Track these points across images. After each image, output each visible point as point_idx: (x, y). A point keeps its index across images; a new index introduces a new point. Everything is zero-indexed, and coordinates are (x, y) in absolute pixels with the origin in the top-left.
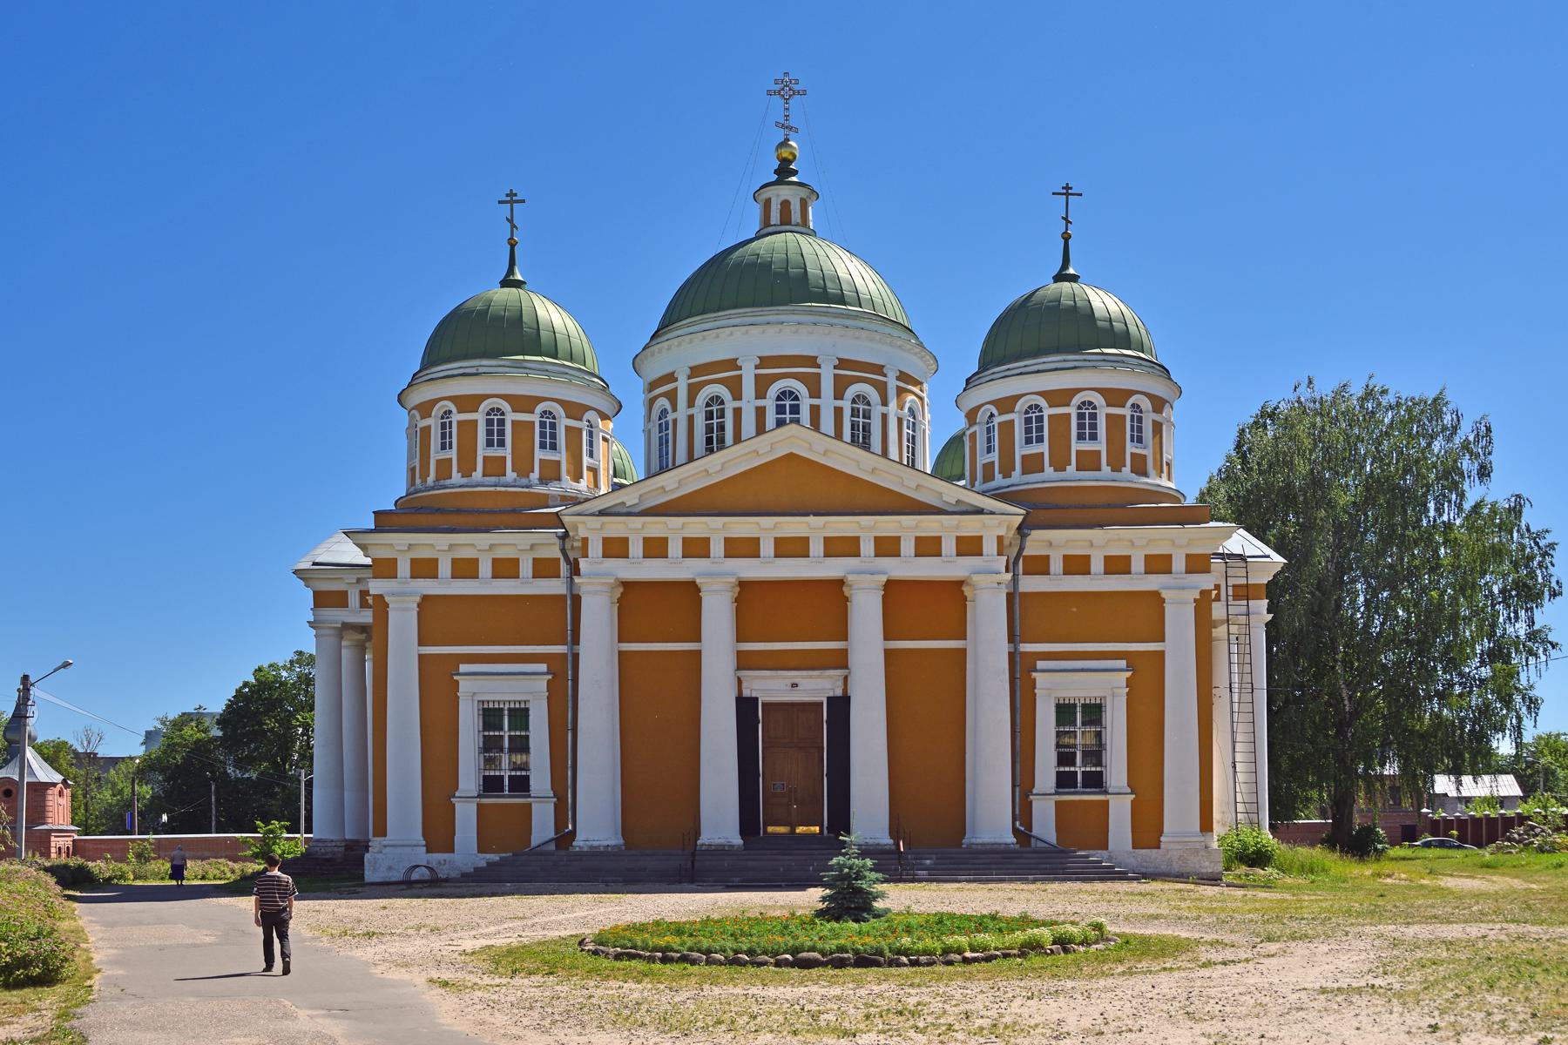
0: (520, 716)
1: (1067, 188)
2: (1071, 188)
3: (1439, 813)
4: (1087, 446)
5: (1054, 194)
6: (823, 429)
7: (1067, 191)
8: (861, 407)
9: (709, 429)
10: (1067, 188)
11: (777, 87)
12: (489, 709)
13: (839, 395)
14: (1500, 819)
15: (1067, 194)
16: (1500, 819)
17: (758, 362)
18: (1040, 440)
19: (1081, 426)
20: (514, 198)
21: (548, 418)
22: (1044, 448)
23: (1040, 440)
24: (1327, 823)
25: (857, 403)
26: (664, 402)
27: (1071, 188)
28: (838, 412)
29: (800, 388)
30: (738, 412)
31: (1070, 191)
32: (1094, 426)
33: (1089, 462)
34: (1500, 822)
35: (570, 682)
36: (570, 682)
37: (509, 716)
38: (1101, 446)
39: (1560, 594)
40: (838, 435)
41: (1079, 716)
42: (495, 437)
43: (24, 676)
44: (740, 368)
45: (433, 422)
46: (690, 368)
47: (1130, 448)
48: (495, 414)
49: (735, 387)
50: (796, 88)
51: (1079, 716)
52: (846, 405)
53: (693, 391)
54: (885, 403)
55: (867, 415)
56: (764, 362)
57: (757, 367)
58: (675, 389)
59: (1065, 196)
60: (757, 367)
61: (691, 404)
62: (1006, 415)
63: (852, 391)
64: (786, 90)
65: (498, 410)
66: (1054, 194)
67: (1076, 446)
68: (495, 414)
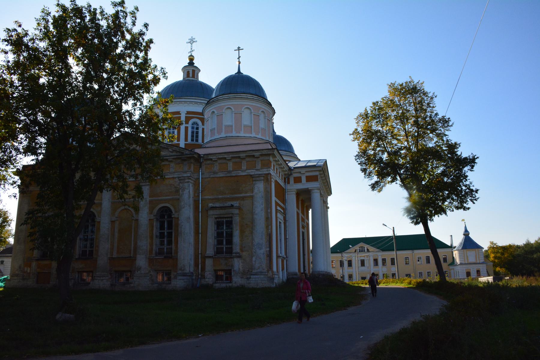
1: (239, 48)
2: (240, 48)
3: (112, 95)
5: (235, 50)
7: (239, 49)
8: (195, 126)
9: (193, 132)
10: (239, 48)
11: (189, 41)
13: (187, 122)
15: (239, 50)
17: (186, 112)
20: (240, 49)
24: (201, 212)
25: (194, 125)
27: (240, 48)
31: (240, 49)
37: (165, 228)
39: (409, 264)
41: (225, 235)
44: (180, 114)
46: (187, 111)
50: (194, 40)
51: (225, 235)
52: (190, 125)
53: (187, 120)
54: (203, 125)
55: (197, 128)
56: (188, 113)
59: (238, 51)
60: (186, 114)
64: (192, 41)
65: (196, 123)
66: (235, 50)
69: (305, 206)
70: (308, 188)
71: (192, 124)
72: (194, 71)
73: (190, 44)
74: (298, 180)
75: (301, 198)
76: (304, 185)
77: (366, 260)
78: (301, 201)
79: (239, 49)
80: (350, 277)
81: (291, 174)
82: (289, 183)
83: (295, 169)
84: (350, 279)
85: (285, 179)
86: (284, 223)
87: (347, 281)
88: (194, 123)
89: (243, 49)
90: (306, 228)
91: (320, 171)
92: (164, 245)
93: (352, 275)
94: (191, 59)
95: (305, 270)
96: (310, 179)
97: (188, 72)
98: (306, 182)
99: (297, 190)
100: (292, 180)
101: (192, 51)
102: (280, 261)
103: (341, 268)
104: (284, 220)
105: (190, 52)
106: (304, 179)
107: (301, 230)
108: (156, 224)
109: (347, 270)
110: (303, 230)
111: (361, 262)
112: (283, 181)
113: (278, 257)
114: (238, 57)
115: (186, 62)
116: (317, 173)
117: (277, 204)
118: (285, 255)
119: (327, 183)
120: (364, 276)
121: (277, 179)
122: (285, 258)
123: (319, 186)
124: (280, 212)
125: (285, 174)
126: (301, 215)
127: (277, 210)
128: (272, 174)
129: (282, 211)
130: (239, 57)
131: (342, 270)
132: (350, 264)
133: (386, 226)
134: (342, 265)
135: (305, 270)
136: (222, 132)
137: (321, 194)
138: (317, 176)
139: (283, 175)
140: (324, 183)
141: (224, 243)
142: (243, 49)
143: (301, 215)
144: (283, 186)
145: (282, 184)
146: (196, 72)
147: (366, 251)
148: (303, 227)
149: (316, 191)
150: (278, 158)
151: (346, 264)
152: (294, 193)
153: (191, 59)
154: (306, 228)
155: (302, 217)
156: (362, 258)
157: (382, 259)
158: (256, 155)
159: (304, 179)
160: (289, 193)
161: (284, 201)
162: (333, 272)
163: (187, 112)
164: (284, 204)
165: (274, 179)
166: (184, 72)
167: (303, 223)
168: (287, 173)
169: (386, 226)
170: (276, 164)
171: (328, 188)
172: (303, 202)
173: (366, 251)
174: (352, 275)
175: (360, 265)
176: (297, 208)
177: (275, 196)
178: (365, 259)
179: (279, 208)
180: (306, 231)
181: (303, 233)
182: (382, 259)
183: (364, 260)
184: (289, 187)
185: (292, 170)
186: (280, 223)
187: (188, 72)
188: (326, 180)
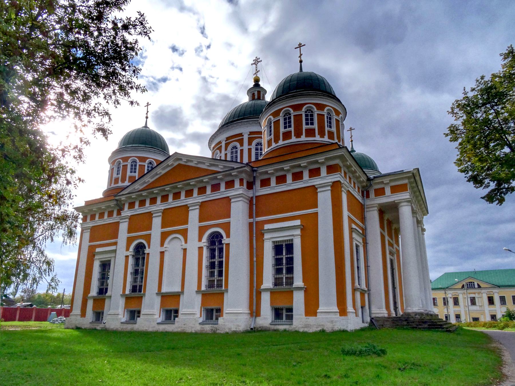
0: (290, 247)
1: (300, 44)
4: (310, 126)
6: (115, 249)
10: (300, 44)
11: (254, 62)
12: (277, 278)
14: (254, 217)
16: (254, 217)
17: (249, 133)
18: (135, 172)
19: (307, 120)
21: (309, 112)
22: (292, 129)
23: (135, 172)
26: (218, 151)
28: (250, 150)
29: (238, 144)
30: (242, 151)
32: (312, 120)
33: (310, 133)
34: (254, 215)
35: (254, 203)
36: (254, 203)
38: (316, 126)
40: (115, 244)
42: (134, 170)
43: (252, 188)
45: (129, 163)
47: (327, 129)
48: (309, 110)
49: (241, 142)
50: (259, 60)
53: (227, 145)
56: (251, 133)
57: (249, 135)
58: (221, 146)
61: (226, 149)
62: (278, 224)
63: (254, 143)
67: (305, 127)
68: (309, 110)
69: (393, 228)
70: (394, 201)
71: (256, 145)
72: (259, 92)
73: (254, 65)
74: (380, 192)
75: (386, 217)
76: (388, 198)
77: (478, 298)
78: (387, 220)
79: (300, 46)
80: (458, 317)
81: (371, 185)
82: (368, 196)
83: (376, 179)
84: (457, 319)
85: (363, 192)
86: (364, 246)
87: (453, 320)
88: (258, 144)
89: (305, 45)
90: (395, 255)
91: (409, 178)
92: (214, 276)
93: (459, 315)
94: (257, 81)
95: (397, 308)
96: (395, 189)
97: (254, 94)
98: (392, 193)
99: (379, 204)
100: (372, 194)
101: (258, 72)
102: (358, 295)
103: (445, 307)
104: (363, 242)
105: (255, 73)
106: (388, 190)
107: (388, 257)
108: (206, 253)
109: (452, 310)
110: (392, 257)
111: (471, 300)
112: (361, 194)
113: (354, 290)
114: (299, 55)
115: (252, 84)
116: (406, 181)
117: (351, 221)
118: (366, 287)
119: (415, 183)
120: (476, 317)
121: (349, 189)
122: (366, 291)
123: (408, 197)
124: (356, 231)
125: (363, 187)
126: (387, 238)
127: (351, 230)
128: (342, 182)
129: (361, 231)
130: (301, 55)
131: (446, 309)
132: (456, 302)
133: (511, 251)
134: (446, 303)
135: (397, 308)
136: (279, 139)
137: (413, 210)
138: (406, 185)
139: (360, 187)
140: (415, 192)
141: (284, 272)
142: (305, 45)
143: (387, 238)
144: (361, 201)
145: (359, 198)
146: (262, 93)
147: (476, 286)
148: (391, 253)
149: (405, 204)
150: (354, 167)
151: (451, 302)
152: (376, 208)
153: (257, 81)
154: (395, 255)
155: (388, 241)
156: (473, 295)
157: (500, 297)
158: (396, 200)
159: (388, 190)
160: (368, 210)
161: (363, 219)
162: (435, 310)
163: (250, 132)
164: (363, 223)
165: (345, 189)
166: (249, 96)
167: (391, 248)
168: (365, 184)
169: (511, 251)
170: (353, 176)
171: (420, 195)
172: (390, 223)
173: (476, 286)
174: (459, 315)
175: (470, 304)
176: (380, 227)
177: (349, 210)
178: (476, 296)
179: (354, 226)
180: (396, 258)
181: (392, 261)
182: (500, 297)
183: (474, 298)
184: (368, 202)
185: (372, 180)
186: (357, 246)
187: (254, 94)
188: (415, 178)
